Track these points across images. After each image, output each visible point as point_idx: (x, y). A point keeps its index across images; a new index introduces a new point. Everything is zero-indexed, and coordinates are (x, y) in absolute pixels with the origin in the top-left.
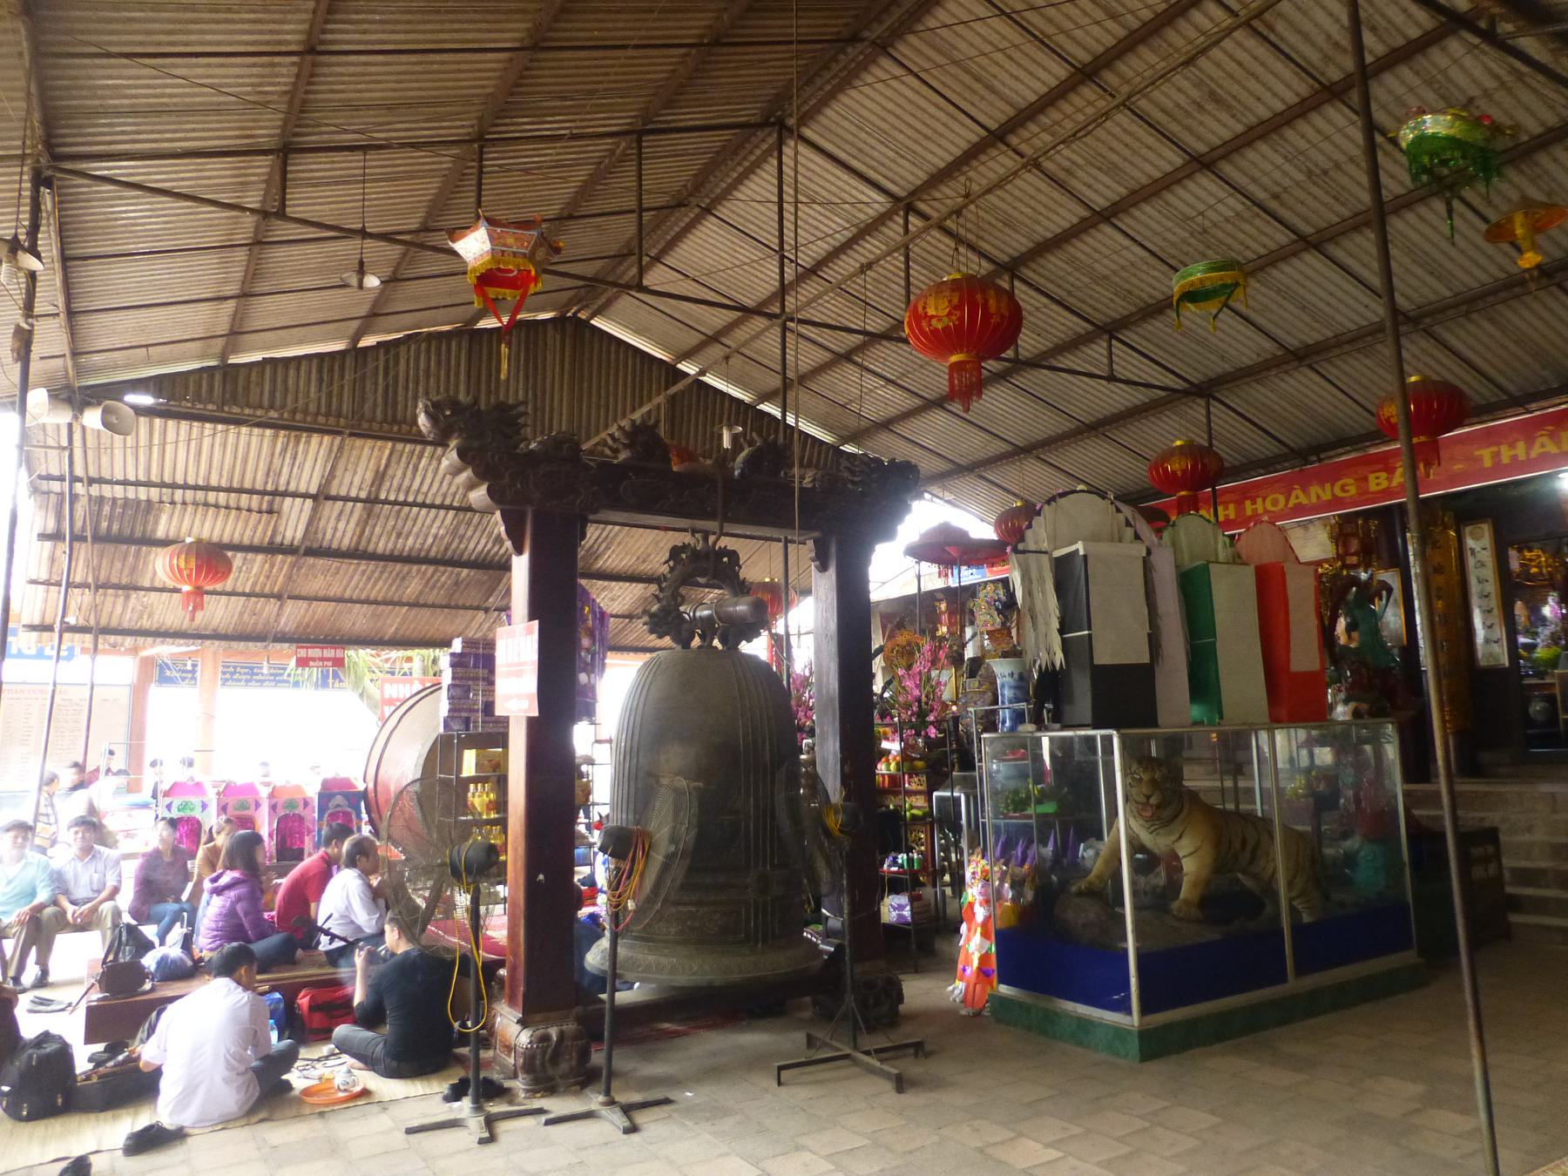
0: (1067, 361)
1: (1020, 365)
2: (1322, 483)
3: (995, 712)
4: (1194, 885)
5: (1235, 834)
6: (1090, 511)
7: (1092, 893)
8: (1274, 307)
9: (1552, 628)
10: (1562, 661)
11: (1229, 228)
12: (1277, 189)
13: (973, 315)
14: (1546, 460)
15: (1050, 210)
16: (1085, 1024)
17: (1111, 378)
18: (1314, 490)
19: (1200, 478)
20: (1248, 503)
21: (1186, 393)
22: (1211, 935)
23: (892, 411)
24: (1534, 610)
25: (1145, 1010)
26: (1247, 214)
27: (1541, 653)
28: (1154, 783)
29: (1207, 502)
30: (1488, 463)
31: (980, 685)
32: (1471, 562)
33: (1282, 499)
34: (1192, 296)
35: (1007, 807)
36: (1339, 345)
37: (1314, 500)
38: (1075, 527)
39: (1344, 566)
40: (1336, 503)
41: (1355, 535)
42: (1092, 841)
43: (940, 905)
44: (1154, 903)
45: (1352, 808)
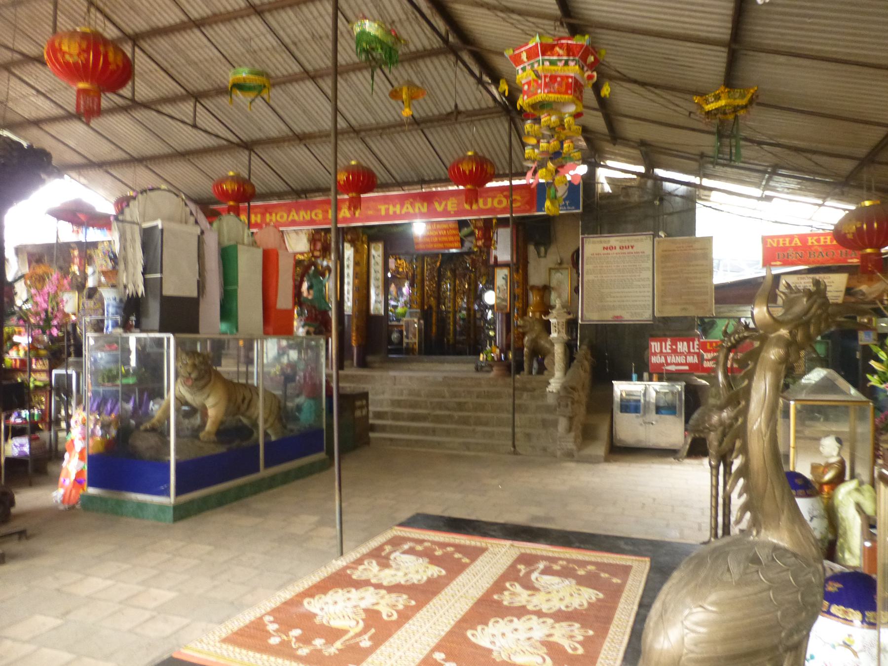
0: (168, 109)
1: (134, 105)
2: (306, 209)
3: (102, 321)
4: (214, 423)
5: (239, 395)
6: (167, 203)
7: (153, 429)
8: (289, 107)
9: (405, 298)
10: (407, 314)
11: (268, 53)
12: (296, 40)
13: (96, 59)
14: (407, 215)
15: (162, 8)
16: (141, 506)
17: (195, 126)
18: (302, 213)
19: (243, 195)
20: (268, 215)
21: (238, 145)
22: (221, 449)
23: (42, 114)
24: (399, 289)
25: (178, 492)
26: (279, 49)
27: (400, 310)
28: (194, 366)
29: (244, 209)
30: (383, 213)
31: (95, 304)
32: (372, 261)
33: (285, 216)
34: (239, 86)
35: (103, 379)
36: (320, 137)
37: (301, 218)
38: (160, 211)
39: (313, 256)
40: (312, 222)
41: (320, 240)
42: (159, 400)
43: (53, 445)
44: (189, 435)
45: (302, 381)
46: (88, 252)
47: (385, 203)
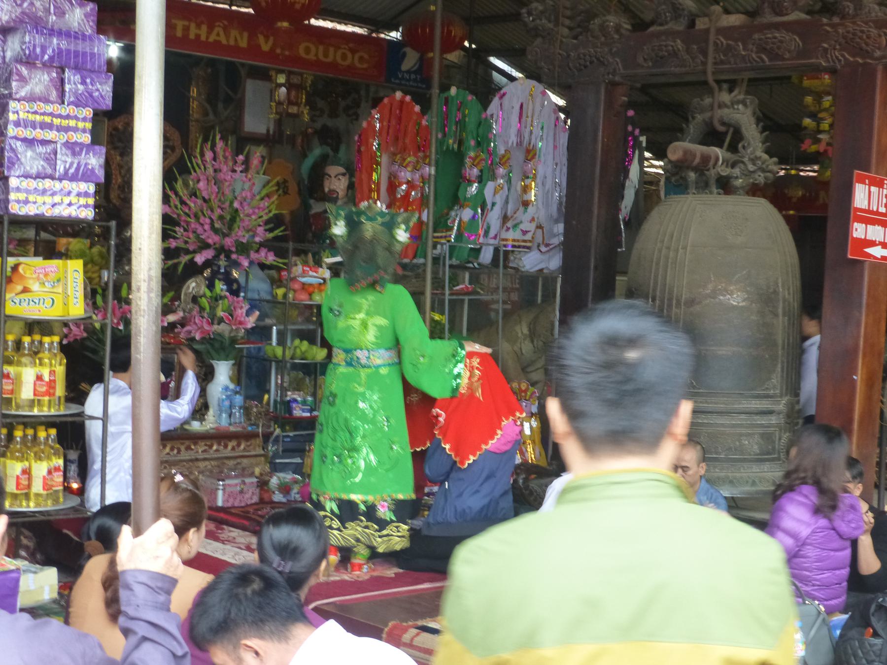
46: (807, 489)
47: (185, 18)
